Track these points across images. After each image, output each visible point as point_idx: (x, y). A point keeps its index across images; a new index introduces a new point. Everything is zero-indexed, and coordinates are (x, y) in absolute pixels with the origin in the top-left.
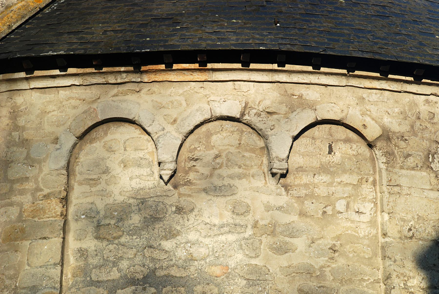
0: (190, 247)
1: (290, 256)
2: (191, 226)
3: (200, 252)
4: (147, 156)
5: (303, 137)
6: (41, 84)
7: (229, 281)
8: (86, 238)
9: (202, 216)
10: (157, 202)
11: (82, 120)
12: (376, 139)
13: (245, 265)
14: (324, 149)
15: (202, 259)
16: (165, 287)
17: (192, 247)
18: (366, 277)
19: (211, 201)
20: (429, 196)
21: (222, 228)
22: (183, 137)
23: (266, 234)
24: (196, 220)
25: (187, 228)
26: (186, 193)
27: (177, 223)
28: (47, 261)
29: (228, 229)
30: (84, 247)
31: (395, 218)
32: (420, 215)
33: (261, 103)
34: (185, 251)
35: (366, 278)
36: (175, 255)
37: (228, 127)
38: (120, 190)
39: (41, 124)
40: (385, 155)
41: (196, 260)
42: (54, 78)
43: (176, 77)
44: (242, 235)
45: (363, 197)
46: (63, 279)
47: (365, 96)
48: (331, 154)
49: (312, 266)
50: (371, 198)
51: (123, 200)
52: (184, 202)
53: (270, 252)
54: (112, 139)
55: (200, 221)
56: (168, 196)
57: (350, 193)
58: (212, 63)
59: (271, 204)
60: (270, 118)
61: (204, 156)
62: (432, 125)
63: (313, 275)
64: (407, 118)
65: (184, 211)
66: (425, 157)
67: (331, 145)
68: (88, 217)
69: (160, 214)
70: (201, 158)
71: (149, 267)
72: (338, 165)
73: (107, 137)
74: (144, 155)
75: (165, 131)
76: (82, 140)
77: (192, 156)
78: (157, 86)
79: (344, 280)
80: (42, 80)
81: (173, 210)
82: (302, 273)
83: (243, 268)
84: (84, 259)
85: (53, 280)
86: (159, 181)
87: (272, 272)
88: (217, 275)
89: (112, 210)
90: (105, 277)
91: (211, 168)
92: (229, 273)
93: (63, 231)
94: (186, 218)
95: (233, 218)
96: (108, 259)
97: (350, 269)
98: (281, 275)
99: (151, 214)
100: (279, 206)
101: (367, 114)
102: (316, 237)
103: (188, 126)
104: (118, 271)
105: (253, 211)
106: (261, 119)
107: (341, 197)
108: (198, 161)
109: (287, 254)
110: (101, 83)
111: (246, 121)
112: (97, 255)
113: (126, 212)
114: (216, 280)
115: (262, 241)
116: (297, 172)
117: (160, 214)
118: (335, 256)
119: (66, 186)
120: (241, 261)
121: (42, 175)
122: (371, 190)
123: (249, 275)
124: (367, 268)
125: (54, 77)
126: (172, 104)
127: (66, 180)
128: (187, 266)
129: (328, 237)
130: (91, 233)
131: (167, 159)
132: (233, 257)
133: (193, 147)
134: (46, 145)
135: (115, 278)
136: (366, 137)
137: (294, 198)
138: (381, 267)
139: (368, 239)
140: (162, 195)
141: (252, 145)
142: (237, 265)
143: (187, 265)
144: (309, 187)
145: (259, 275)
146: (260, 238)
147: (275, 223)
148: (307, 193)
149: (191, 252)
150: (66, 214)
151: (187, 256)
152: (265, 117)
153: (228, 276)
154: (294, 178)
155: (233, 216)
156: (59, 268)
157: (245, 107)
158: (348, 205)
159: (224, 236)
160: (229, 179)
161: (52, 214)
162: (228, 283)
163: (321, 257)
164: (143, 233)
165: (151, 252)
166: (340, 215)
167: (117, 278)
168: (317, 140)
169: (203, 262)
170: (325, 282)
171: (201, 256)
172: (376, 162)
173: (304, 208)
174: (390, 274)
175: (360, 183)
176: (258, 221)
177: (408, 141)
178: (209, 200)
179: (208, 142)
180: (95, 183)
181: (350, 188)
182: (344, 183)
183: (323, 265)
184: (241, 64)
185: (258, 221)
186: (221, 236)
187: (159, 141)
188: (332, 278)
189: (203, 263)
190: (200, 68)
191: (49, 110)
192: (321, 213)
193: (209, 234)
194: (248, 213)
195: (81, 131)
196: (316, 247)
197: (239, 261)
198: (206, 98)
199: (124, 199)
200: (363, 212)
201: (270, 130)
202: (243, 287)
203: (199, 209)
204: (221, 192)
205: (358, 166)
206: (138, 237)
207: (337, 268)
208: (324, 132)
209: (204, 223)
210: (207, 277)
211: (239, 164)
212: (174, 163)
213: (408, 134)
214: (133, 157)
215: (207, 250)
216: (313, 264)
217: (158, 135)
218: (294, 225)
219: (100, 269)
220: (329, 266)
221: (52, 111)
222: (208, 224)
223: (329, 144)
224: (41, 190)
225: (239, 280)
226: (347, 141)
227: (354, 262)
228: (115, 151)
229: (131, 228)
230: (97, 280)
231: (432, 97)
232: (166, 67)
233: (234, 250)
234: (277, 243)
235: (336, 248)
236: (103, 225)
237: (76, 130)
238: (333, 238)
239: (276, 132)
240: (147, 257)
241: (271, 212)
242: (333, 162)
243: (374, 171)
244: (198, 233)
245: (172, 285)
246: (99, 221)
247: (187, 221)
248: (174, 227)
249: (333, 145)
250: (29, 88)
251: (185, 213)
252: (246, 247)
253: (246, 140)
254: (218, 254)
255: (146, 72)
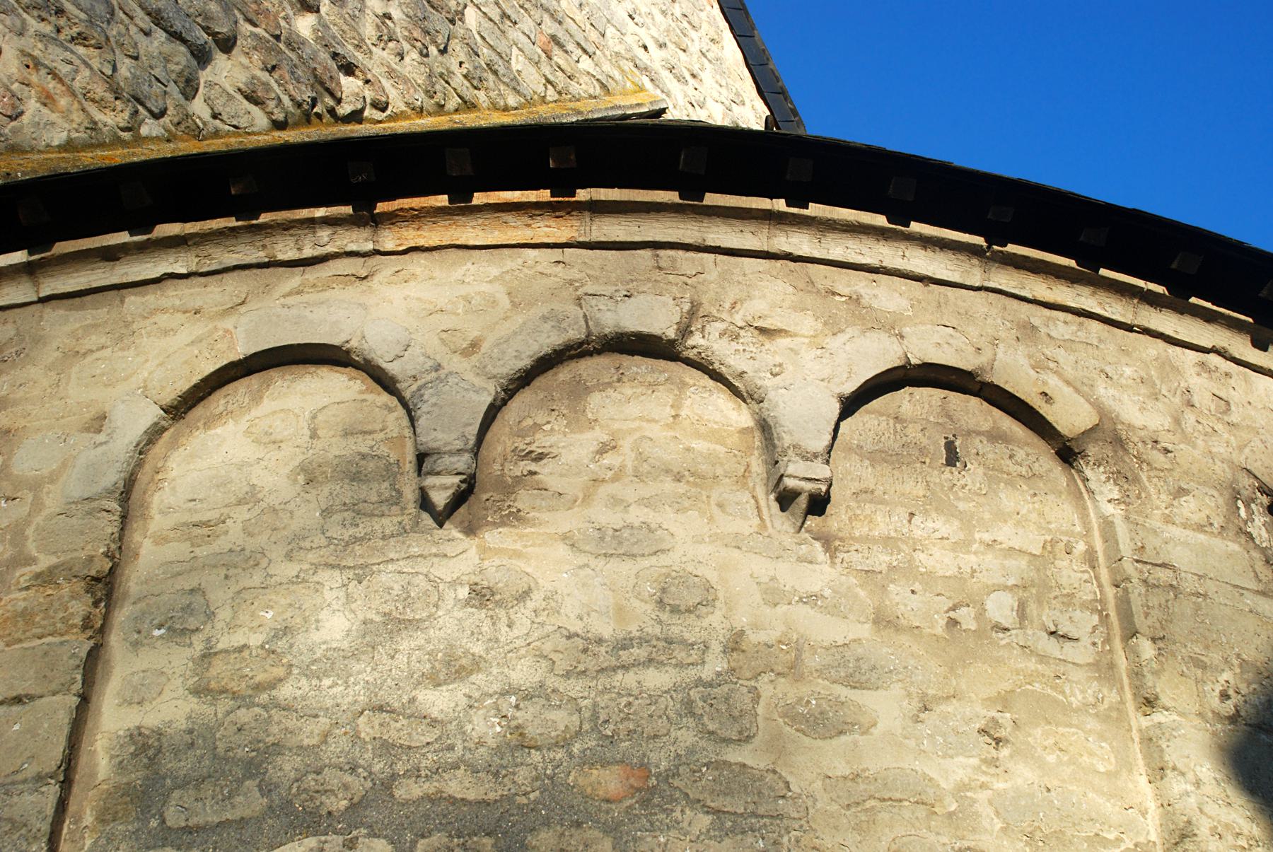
0: (517, 707)
1: (855, 743)
2: (519, 643)
3: (550, 723)
4: (382, 448)
5: (868, 412)
6: (72, 281)
7: (651, 814)
8: (162, 696)
9: (558, 612)
10: (409, 573)
11: (186, 362)
12: (1083, 433)
13: (707, 765)
14: (932, 452)
15: (556, 744)
16: (423, 836)
17: (522, 705)
18: (1109, 831)
19: (588, 571)
20: (1260, 610)
21: (624, 648)
22: (499, 390)
23: (772, 671)
24: (536, 626)
25: (506, 648)
26: (505, 546)
27: (473, 633)
28: (12, 770)
29: (646, 654)
30: (150, 725)
31: (1173, 655)
32: (1244, 656)
33: (738, 306)
34: (498, 720)
35: (1111, 836)
36: (464, 733)
37: (637, 373)
38: (290, 547)
39: (58, 386)
40: (1114, 481)
41: (538, 748)
42: (113, 260)
43: (481, 233)
44: (692, 673)
45: (1065, 592)
46: (65, 831)
47: (1036, 321)
48: (955, 466)
49: (931, 779)
50: (1089, 598)
51: (295, 573)
52: (497, 571)
53: (788, 728)
54: (275, 412)
55: (551, 629)
56: (446, 556)
57: (1025, 576)
58: (591, 187)
59: (782, 586)
60: (767, 346)
61: (564, 447)
62: (1227, 427)
63: (936, 810)
64: (1160, 397)
65: (498, 597)
66: (1227, 505)
67: (953, 442)
68: (175, 631)
69: (418, 609)
70: (555, 451)
71: (370, 773)
72: (979, 495)
73: (260, 408)
74: (371, 447)
75: (441, 372)
76: (182, 421)
77: (525, 447)
78: (422, 261)
79: (1041, 834)
80: (77, 271)
81: (461, 596)
82: (901, 801)
83: (697, 774)
84: (146, 761)
85: (23, 831)
86: (418, 516)
87: (799, 791)
88: (608, 796)
89: (256, 604)
90: (215, 812)
91: (586, 478)
92: (652, 790)
93: (84, 675)
94: (504, 619)
95: (660, 622)
96: (231, 754)
97: (1052, 802)
98: (830, 804)
99: (387, 611)
100: (809, 593)
101: (1049, 368)
102: (934, 692)
103: (516, 357)
104: (261, 790)
105: (726, 603)
106: (741, 348)
107: (999, 585)
108: (545, 461)
109: (843, 738)
110: (254, 261)
111: (695, 351)
112: (192, 744)
113: (304, 608)
114: (607, 812)
115: (758, 694)
116: (858, 502)
117: (418, 609)
118: (1001, 755)
119: (113, 546)
120: (691, 751)
121: (39, 519)
122: (1086, 576)
123: (721, 798)
124: (1108, 804)
125: (111, 255)
126: (467, 305)
127: (116, 530)
128: (505, 767)
129: (972, 695)
130: (182, 679)
131: (446, 444)
132: (665, 739)
133: (529, 422)
134: (63, 437)
135: (247, 813)
136: (1055, 424)
137: (855, 572)
138: (1152, 805)
139: (1097, 715)
140: (426, 553)
141: (716, 423)
142: (677, 762)
143: (504, 762)
144: (898, 546)
145: (756, 798)
146: (752, 683)
147: (798, 639)
148: (895, 564)
149: (520, 721)
150: (102, 626)
151: (505, 736)
152: (754, 344)
153: (649, 800)
154: (850, 518)
155: (661, 615)
156: (52, 791)
157: (692, 313)
158: (1023, 610)
159: (631, 673)
160: (646, 510)
161: (54, 624)
162: (648, 821)
163: (957, 755)
164: (358, 667)
165: (381, 725)
166: (1001, 635)
167: (256, 815)
168: (910, 426)
169: (560, 755)
170: (977, 837)
171: (553, 734)
172: (1089, 503)
173: (888, 603)
174: (1189, 822)
175: (1050, 552)
176: (742, 633)
177: (1172, 455)
178: (580, 567)
179: (576, 412)
180: (209, 533)
181: (1023, 562)
182: (1004, 546)
183: (966, 781)
184: (677, 193)
185: (742, 633)
186: (620, 672)
187: (422, 396)
188: (999, 825)
189: (559, 756)
190: (556, 199)
191: (88, 347)
192: (943, 622)
193: (581, 667)
194: (710, 609)
195: (179, 389)
196: (938, 722)
197: (683, 752)
198: (571, 289)
199: (301, 569)
200: (1070, 635)
201: (769, 375)
202: (702, 837)
203: (549, 594)
204: (620, 543)
205: (1036, 506)
206: (340, 682)
207: (1012, 794)
208: (927, 406)
209: (565, 633)
210: (575, 802)
211: (676, 470)
212: (467, 457)
213: (1170, 435)
214: (337, 453)
215: (575, 718)
216: (932, 775)
217: (419, 383)
218: (859, 650)
219: (197, 788)
220: (983, 786)
221: (98, 350)
222: (578, 636)
223: (946, 438)
224: (31, 561)
225: (688, 812)
226: (995, 436)
227: (1063, 781)
228: (281, 442)
229: (318, 655)
230: (183, 824)
231: (1214, 359)
232: (450, 201)
233: (668, 718)
234: (808, 702)
235: (1002, 733)
236: (221, 652)
237: (163, 388)
238: (989, 699)
239: (788, 382)
240: (367, 739)
241: (786, 607)
242: (963, 488)
243: (1085, 527)
244: (544, 663)
245: (449, 828)
246: (210, 642)
247: (508, 629)
248: (461, 646)
249: (957, 443)
250: (35, 299)
251: (499, 604)
252: (707, 709)
253: (696, 406)
254: (612, 727)
255: (392, 219)
